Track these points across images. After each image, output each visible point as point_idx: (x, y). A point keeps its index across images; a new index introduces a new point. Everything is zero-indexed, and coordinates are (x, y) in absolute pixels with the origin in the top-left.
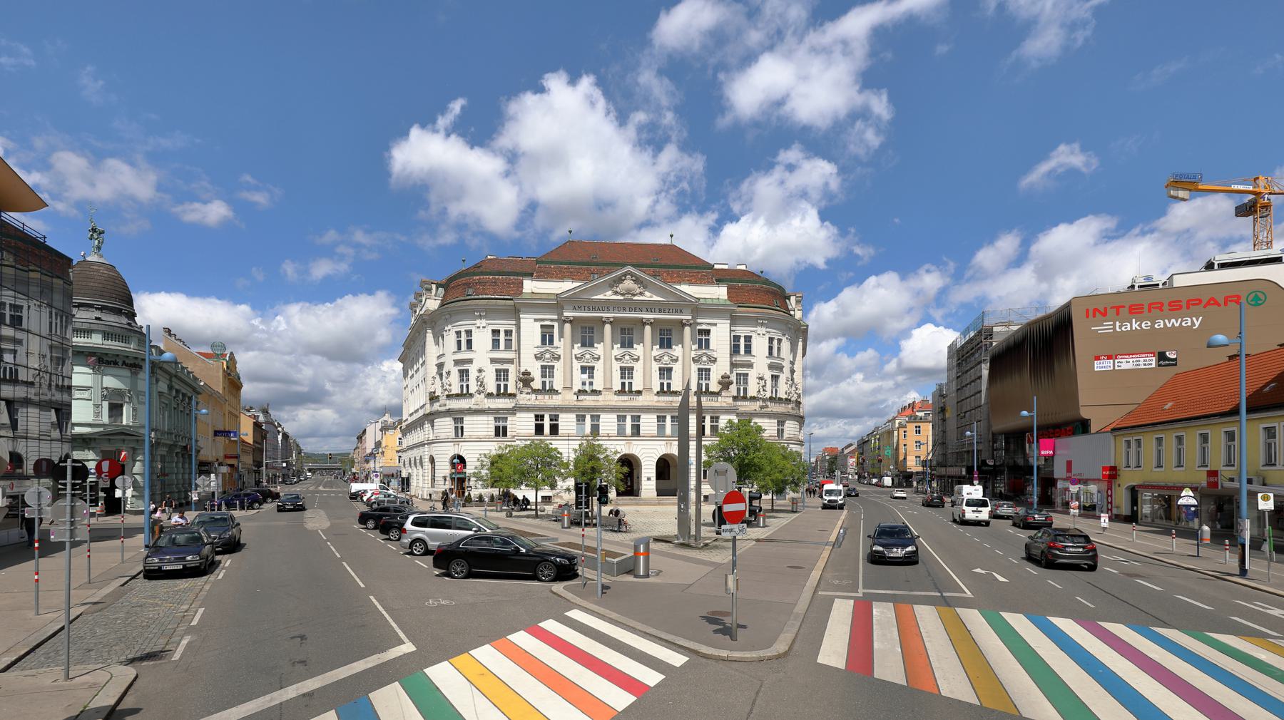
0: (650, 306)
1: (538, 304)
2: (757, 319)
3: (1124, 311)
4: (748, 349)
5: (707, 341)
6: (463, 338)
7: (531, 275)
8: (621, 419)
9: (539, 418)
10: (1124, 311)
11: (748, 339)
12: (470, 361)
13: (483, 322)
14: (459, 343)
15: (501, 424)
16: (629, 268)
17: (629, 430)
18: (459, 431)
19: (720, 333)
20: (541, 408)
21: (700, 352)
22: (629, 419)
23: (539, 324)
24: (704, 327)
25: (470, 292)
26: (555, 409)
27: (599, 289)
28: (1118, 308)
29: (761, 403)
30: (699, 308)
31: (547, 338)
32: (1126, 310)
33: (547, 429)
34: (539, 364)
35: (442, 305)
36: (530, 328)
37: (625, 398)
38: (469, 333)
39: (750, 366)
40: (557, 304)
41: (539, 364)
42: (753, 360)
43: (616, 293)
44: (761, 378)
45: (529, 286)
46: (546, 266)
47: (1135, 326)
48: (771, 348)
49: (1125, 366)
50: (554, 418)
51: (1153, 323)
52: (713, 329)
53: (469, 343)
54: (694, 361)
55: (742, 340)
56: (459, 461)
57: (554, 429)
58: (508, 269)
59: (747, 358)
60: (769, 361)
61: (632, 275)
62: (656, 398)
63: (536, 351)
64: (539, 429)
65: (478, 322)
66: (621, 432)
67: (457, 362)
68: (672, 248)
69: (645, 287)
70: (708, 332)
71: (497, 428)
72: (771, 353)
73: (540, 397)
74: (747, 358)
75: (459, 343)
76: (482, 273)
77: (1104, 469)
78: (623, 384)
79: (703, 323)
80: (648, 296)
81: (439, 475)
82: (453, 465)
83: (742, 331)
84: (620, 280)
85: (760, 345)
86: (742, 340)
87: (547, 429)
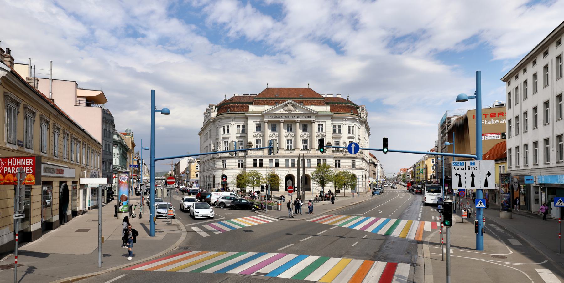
0: (298, 116)
1: (255, 115)
2: (343, 118)
3: (488, 116)
4: (340, 131)
5: (322, 129)
6: (258, 162)
7: (252, 103)
8: (287, 160)
9: (255, 160)
10: (488, 116)
11: (339, 127)
12: (228, 138)
13: (234, 122)
14: (224, 130)
15: (240, 163)
16: (290, 101)
17: (290, 165)
18: (225, 165)
19: (328, 125)
20: (256, 156)
21: (319, 133)
22: (290, 160)
23: (255, 123)
24: (321, 123)
25: (229, 110)
26: (261, 156)
27: (277, 109)
28: (486, 115)
29: (345, 153)
30: (317, 115)
31: (259, 128)
32: (489, 115)
33: (258, 165)
34: (255, 138)
35: (217, 115)
36: (252, 125)
37: (289, 152)
38: (228, 127)
39: (340, 137)
40: (262, 115)
41: (255, 138)
42: (341, 135)
43: (285, 110)
44: (345, 143)
45: (252, 108)
46: (257, 100)
47: (493, 122)
48: (349, 130)
49: (489, 138)
50: (224, 132)
51: (500, 121)
52: (324, 124)
53: (228, 131)
54: (316, 136)
55: (337, 127)
56: (224, 177)
57: (261, 165)
58: (243, 101)
59: (339, 135)
60: (348, 136)
61: (291, 103)
62: (285, 152)
63: (254, 134)
64: (255, 165)
65: (232, 123)
66: (287, 166)
67: (223, 138)
68: (309, 90)
69: (296, 108)
70: (322, 125)
71: (239, 164)
72: (349, 133)
73: (256, 152)
74: (339, 135)
75: (224, 130)
76: (233, 103)
77: (401, 170)
78: (288, 146)
79: (321, 121)
80: (298, 112)
81: (216, 183)
82: (222, 179)
83: (337, 123)
84: (286, 105)
85: (345, 129)
86: (337, 127)
87: (258, 165)
